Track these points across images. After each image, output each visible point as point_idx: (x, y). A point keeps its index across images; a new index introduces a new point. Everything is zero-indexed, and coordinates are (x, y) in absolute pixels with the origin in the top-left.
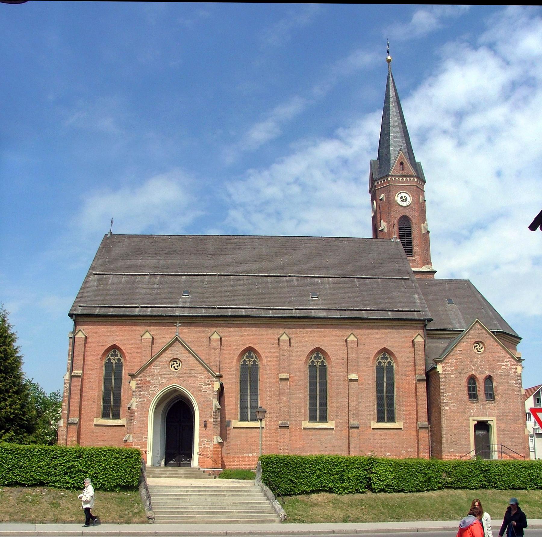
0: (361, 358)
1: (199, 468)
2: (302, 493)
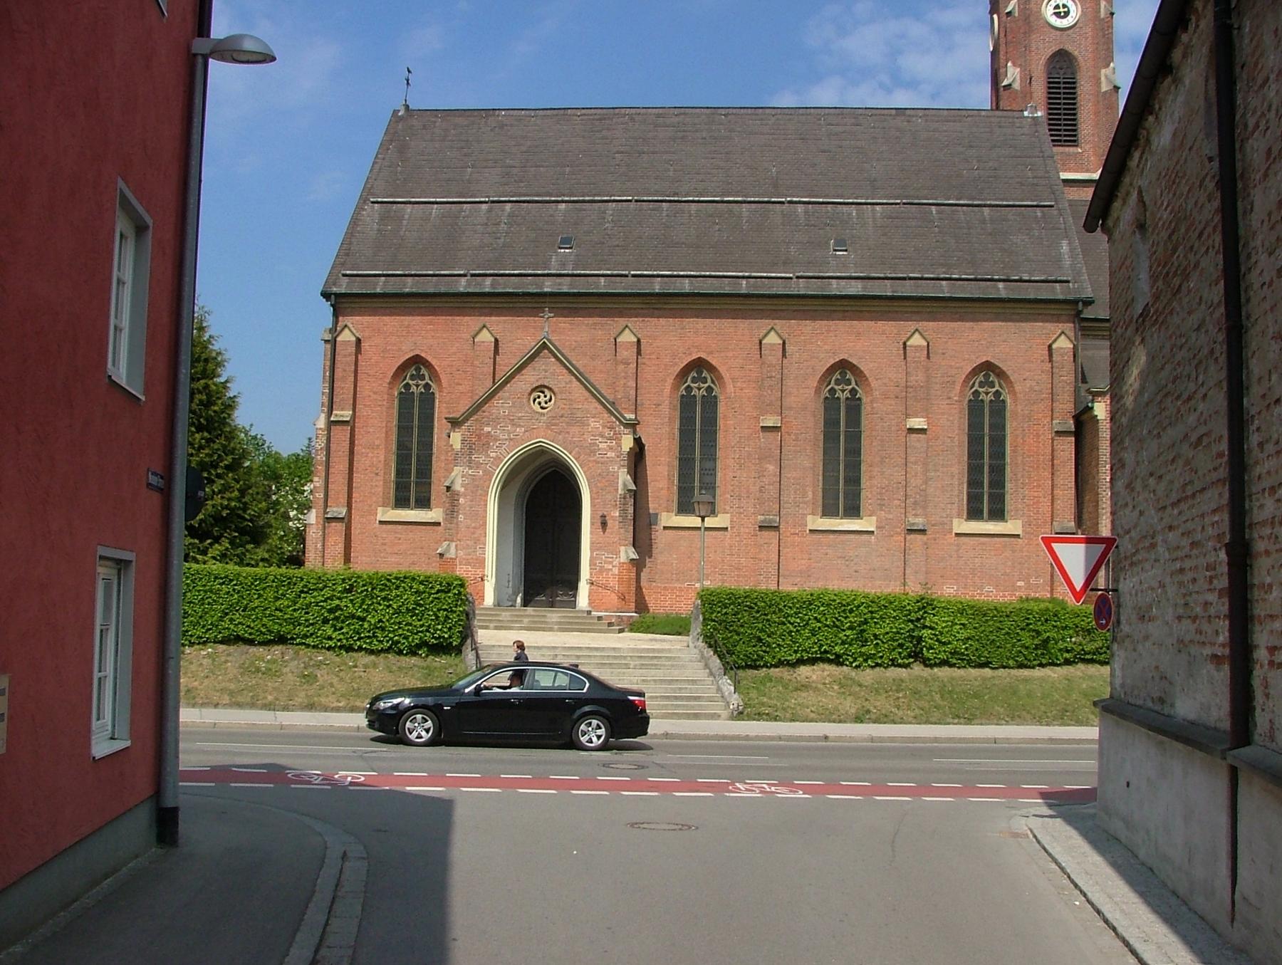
0: (937, 383)
1: (590, 611)
2: (780, 664)
